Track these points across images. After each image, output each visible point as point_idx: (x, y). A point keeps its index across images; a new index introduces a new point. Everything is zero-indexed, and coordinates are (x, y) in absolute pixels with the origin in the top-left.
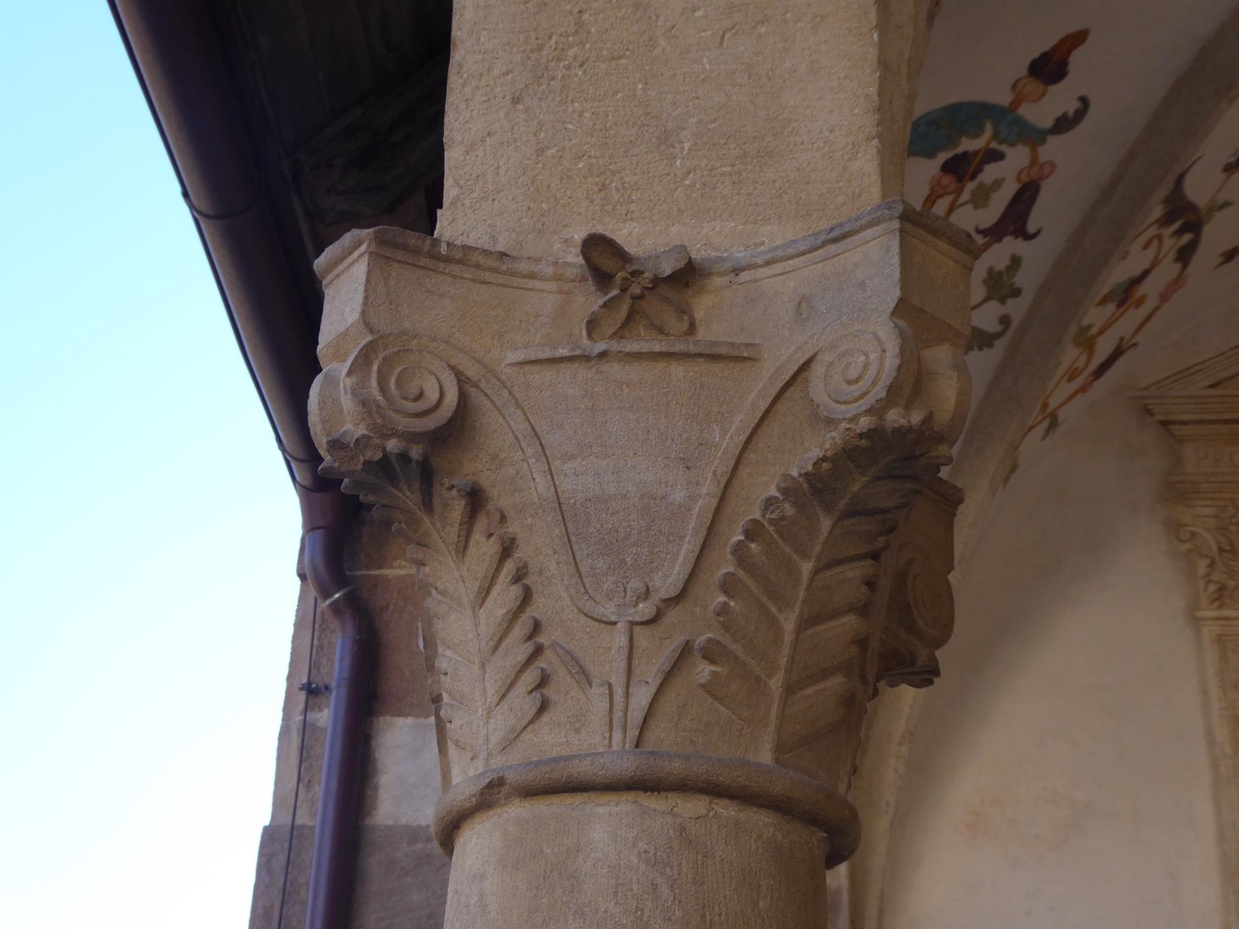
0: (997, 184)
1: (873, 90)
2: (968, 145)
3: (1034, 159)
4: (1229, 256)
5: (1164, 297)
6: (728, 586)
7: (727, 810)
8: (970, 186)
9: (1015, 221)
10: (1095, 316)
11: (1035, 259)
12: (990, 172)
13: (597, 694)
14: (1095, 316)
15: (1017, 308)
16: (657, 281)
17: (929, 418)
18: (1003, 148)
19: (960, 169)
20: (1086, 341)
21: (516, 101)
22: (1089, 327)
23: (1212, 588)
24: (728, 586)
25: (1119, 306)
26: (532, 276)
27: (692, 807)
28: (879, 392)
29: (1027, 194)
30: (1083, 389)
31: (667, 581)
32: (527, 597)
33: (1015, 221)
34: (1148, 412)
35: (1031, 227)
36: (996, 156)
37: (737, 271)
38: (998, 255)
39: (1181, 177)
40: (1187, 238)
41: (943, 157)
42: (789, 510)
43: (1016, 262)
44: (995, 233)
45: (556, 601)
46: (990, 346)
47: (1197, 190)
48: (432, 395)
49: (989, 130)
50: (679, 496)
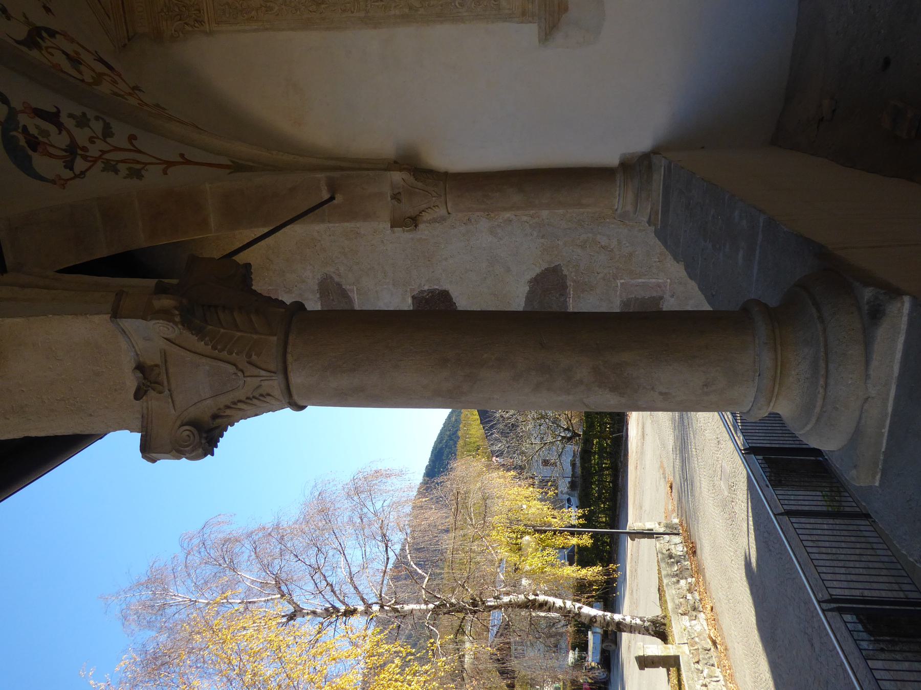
0: (37, 127)
1: (70, 317)
2: (22, 142)
3: (22, 112)
4: (48, 10)
5: (72, 41)
6: (230, 353)
7: (289, 349)
8: (41, 139)
9: (53, 118)
10: (88, 76)
11: (68, 108)
12: (33, 131)
13: (263, 383)
14: (88, 76)
15: (91, 114)
16: (145, 378)
17: (176, 308)
18: (21, 125)
19: (34, 144)
20: (98, 78)
21: (91, 415)
22: (93, 77)
23: (197, 25)
24: (230, 353)
25: (81, 64)
26: (148, 408)
27: (290, 358)
28: (171, 324)
29: (38, 113)
30: (120, 76)
31: (231, 369)
32: (240, 401)
33: (53, 118)
34: (125, 46)
35: (54, 110)
36: (25, 128)
37: (137, 355)
38: (69, 123)
39: (17, 42)
40: (44, 34)
41: (30, 152)
42: (207, 339)
43: (71, 116)
44: (60, 126)
45: (241, 394)
46: (109, 124)
47: (21, 32)
48: (188, 433)
49: (14, 133)
50: (207, 368)
